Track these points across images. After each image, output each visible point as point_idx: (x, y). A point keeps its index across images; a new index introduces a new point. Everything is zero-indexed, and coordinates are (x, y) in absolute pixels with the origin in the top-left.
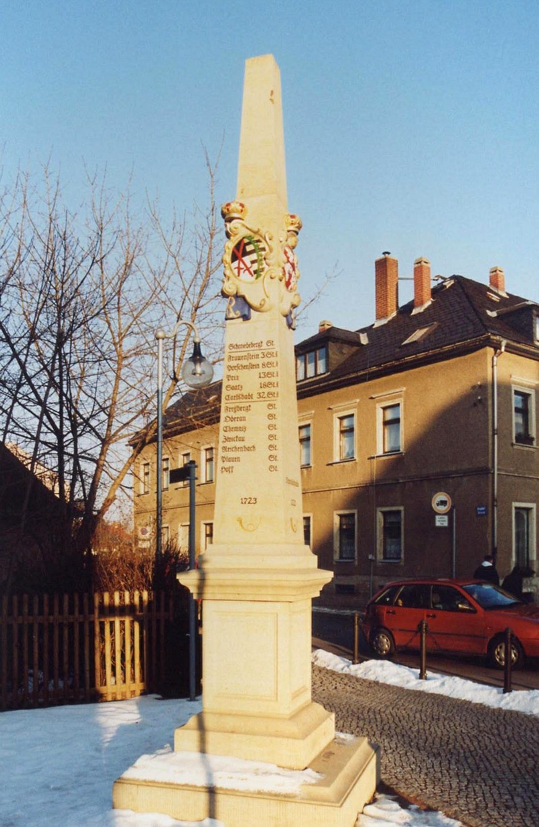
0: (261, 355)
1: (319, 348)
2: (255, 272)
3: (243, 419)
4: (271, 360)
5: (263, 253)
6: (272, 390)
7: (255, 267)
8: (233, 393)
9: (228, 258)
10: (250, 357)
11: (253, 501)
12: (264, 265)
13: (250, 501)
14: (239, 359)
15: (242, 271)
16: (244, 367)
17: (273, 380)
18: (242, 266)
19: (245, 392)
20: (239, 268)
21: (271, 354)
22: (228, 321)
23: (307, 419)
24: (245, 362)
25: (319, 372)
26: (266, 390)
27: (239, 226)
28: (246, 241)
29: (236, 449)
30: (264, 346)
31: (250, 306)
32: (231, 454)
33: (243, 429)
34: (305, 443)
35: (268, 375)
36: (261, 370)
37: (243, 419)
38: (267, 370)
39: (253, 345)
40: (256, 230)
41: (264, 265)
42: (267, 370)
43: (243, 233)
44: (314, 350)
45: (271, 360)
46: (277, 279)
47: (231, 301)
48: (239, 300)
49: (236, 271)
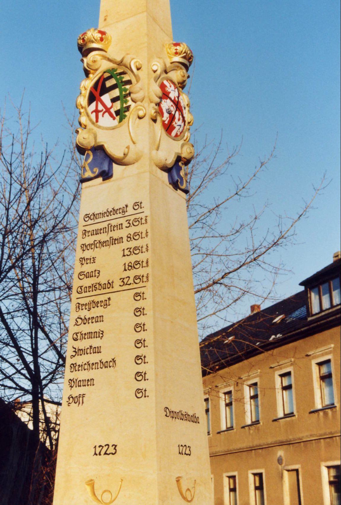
0: (125, 224)
1: (332, 279)
2: (118, 113)
3: (99, 319)
4: (140, 228)
5: (128, 87)
6: (140, 272)
7: (118, 105)
8: (87, 282)
9: (83, 101)
10: (112, 228)
11: (111, 450)
12: (130, 103)
13: (106, 450)
14: (97, 232)
15: (100, 114)
16: (103, 244)
17: (141, 257)
18: (100, 107)
19: (103, 280)
20: (97, 111)
21: (138, 221)
22: (85, 184)
23: (327, 354)
24: (103, 237)
25: (335, 303)
26: (132, 273)
27: (98, 58)
28: (107, 75)
29: (90, 366)
30: (130, 211)
31: (112, 160)
32: (82, 375)
33: (100, 334)
34: (327, 380)
35: (136, 250)
36: (126, 245)
37: (99, 319)
38: (133, 244)
39: (115, 211)
40: (119, 59)
41: (130, 103)
42: (133, 244)
43: (105, 65)
44: (328, 281)
45: (140, 228)
46: (147, 119)
47: (88, 155)
48: (98, 153)
49: (93, 116)
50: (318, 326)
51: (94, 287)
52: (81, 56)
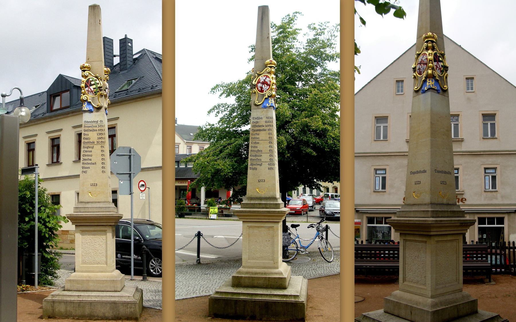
16: (90, 131)
24: (91, 129)
26: (100, 140)
29: (88, 164)
30: (99, 122)
33: (91, 156)
38: (100, 132)
39: (94, 122)
42: (100, 132)
50: (446, 215)
51: (88, 142)
52: (85, 61)
